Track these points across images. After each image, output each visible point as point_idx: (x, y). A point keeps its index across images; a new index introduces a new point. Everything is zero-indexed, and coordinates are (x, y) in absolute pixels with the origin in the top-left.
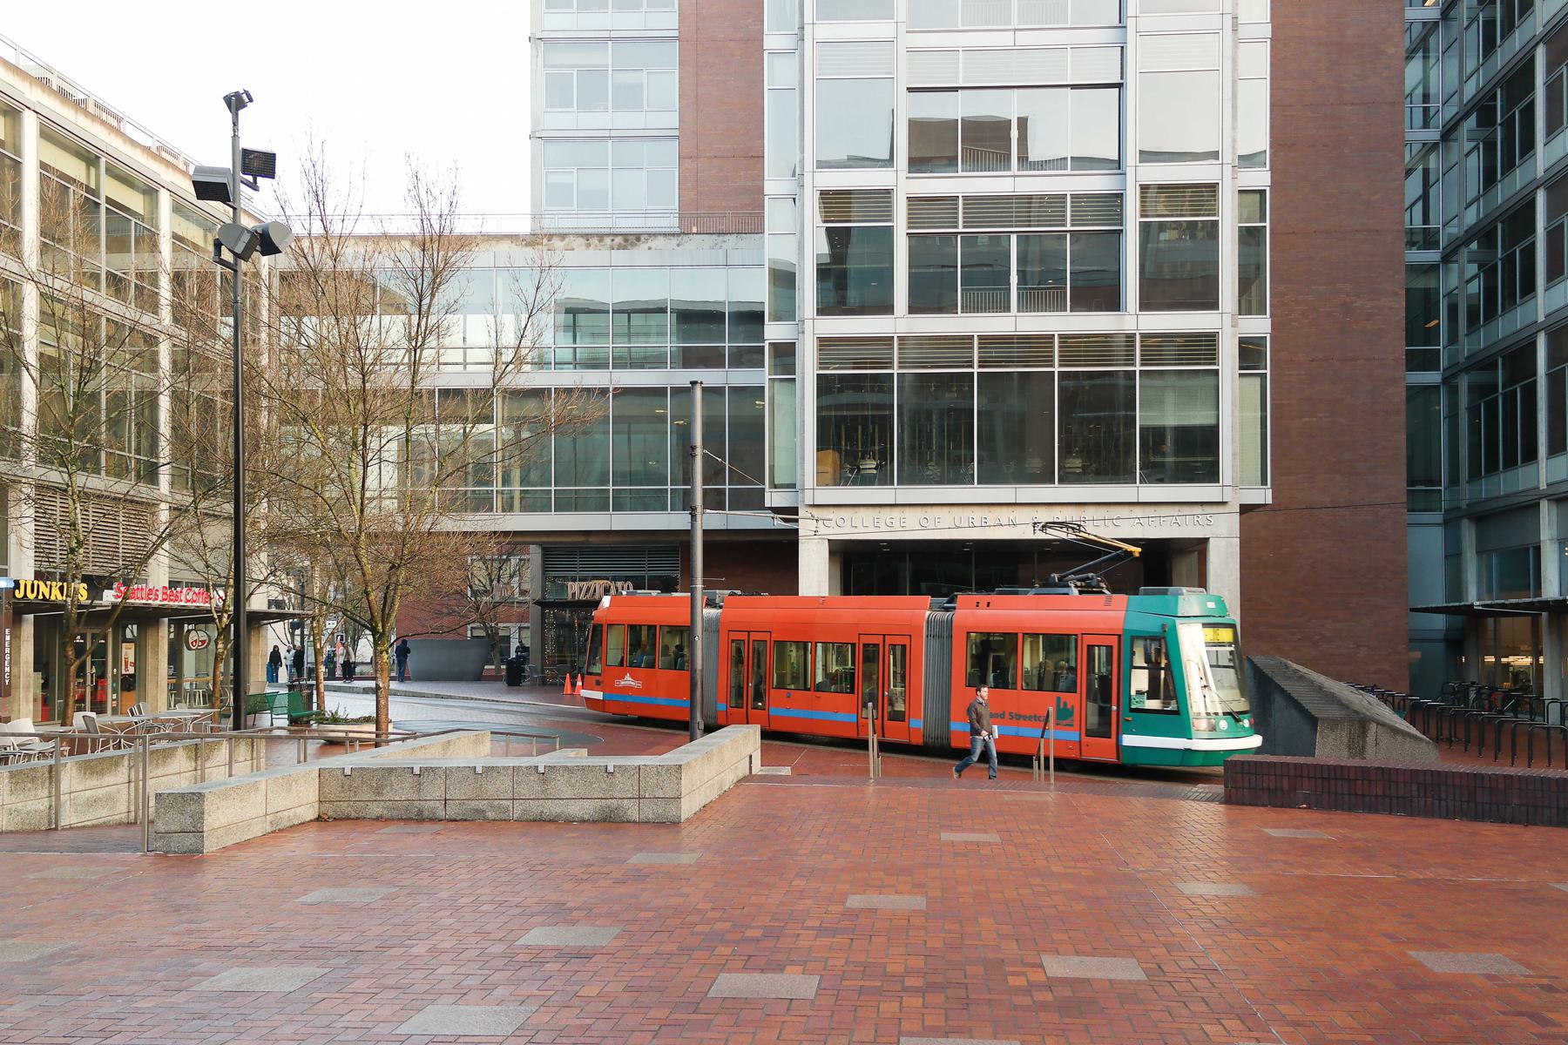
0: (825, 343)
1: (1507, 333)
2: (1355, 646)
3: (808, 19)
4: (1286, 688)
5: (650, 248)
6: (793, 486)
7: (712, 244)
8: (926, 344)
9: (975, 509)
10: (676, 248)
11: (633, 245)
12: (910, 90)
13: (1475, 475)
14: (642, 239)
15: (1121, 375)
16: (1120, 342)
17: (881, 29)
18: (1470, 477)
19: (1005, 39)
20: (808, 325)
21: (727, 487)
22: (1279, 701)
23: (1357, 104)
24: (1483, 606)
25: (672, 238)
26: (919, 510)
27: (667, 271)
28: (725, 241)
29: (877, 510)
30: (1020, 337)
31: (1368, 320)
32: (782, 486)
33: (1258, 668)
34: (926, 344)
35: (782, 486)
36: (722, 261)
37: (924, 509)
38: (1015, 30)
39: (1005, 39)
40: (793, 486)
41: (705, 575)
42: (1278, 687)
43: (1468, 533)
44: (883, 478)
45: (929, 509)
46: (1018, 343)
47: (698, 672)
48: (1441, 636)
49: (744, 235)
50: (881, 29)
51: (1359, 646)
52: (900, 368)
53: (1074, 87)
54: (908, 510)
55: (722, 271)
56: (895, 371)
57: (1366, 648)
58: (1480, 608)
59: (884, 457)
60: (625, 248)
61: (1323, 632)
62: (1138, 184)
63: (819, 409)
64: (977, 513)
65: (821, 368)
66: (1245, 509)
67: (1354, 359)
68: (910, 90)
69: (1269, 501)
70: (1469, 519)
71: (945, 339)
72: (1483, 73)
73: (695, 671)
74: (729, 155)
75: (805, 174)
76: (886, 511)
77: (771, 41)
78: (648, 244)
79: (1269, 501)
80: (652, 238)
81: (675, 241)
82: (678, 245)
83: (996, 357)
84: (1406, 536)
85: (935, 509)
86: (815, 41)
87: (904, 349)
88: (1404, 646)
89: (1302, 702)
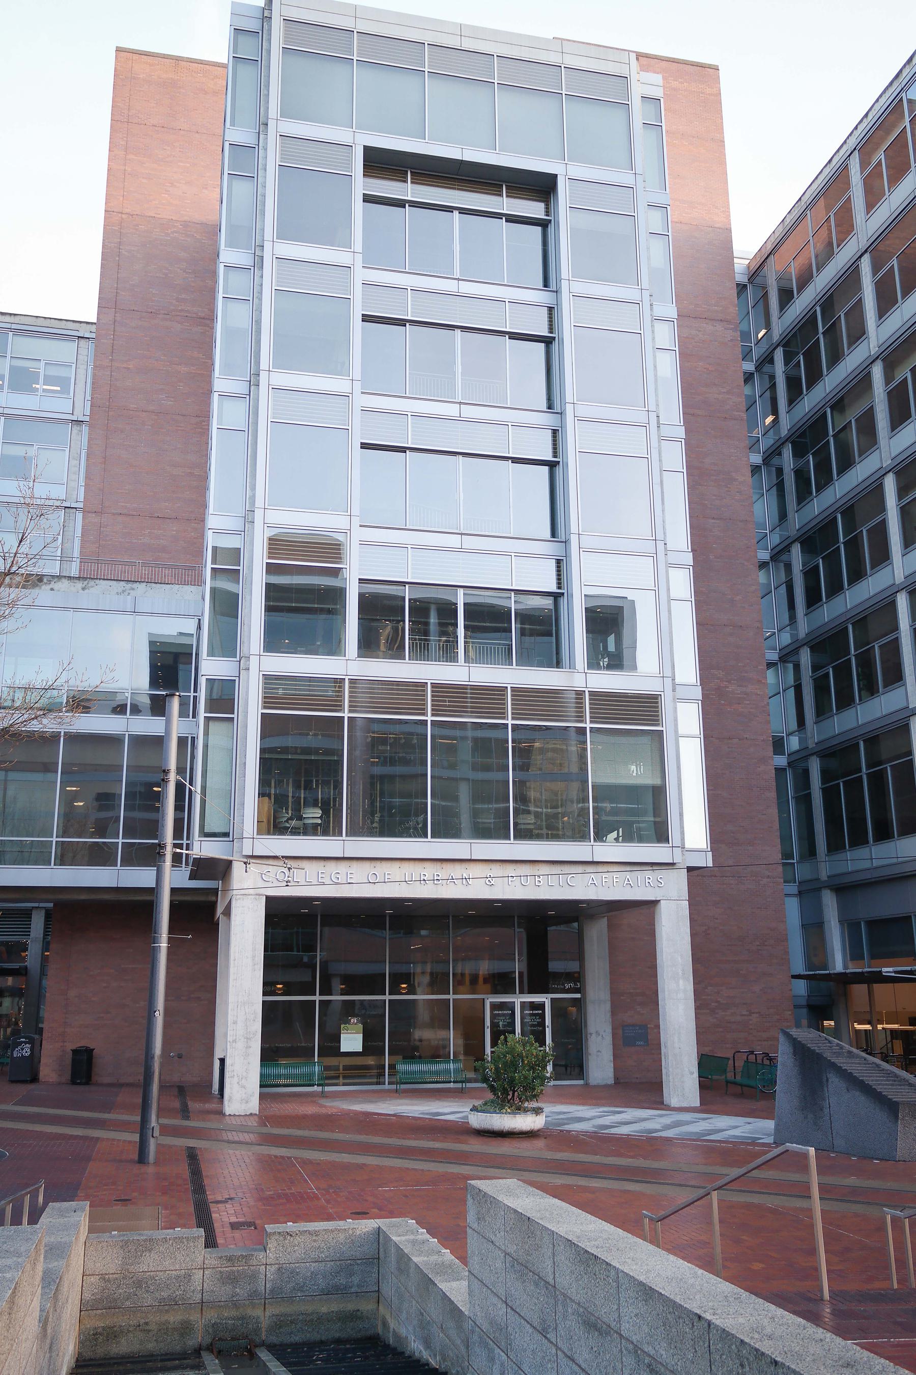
0: (270, 680)
1: (866, 721)
2: (748, 1013)
3: (264, 365)
4: (845, 1067)
5: (52, 589)
6: (226, 835)
7: (120, 590)
8: (379, 689)
9: (428, 865)
10: (81, 591)
11: (34, 586)
12: (364, 446)
13: (835, 846)
14: (45, 580)
15: (573, 731)
16: (571, 698)
17: (339, 385)
18: (829, 851)
19: (452, 410)
20: (254, 662)
21: (120, 841)
22: (834, 1082)
23: (718, 519)
24: (895, 972)
25: (77, 581)
26: (367, 865)
27: (70, 614)
28: (133, 589)
29: (322, 863)
30: (474, 688)
31: (739, 704)
32: (214, 835)
33: (800, 1042)
34: (379, 689)
35: (214, 835)
36: (129, 608)
37: (374, 863)
38: (460, 403)
39: (452, 410)
40: (226, 835)
41: (171, 930)
42: (833, 1066)
43: (830, 903)
44: (326, 828)
45: (378, 864)
46: (471, 698)
47: (156, 1058)
48: (804, 1002)
49: (154, 585)
50: (339, 385)
51: (751, 1013)
52: (350, 711)
53: (515, 460)
54: (355, 864)
55: (129, 618)
56: (346, 715)
57: (757, 1015)
58: (893, 974)
59: (329, 808)
60: (24, 587)
61: (719, 1000)
62: (261, 673)
63: (263, 751)
64: (429, 871)
65: (265, 708)
66: (690, 869)
67: (730, 739)
68: (364, 446)
69: (710, 864)
70: (831, 890)
71: (398, 685)
72: (817, 502)
73: (153, 1057)
74: (135, 513)
75: (256, 510)
76: (331, 865)
77: (220, 384)
78: (51, 586)
79: (710, 864)
80: (56, 580)
81: (79, 585)
82: (83, 589)
83: (449, 706)
84: (784, 904)
85: (385, 864)
86: (567, 177)
87: (355, 692)
88: (790, 1013)
89: (870, 1083)
